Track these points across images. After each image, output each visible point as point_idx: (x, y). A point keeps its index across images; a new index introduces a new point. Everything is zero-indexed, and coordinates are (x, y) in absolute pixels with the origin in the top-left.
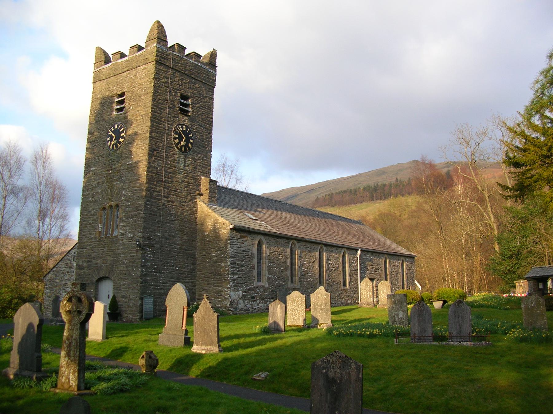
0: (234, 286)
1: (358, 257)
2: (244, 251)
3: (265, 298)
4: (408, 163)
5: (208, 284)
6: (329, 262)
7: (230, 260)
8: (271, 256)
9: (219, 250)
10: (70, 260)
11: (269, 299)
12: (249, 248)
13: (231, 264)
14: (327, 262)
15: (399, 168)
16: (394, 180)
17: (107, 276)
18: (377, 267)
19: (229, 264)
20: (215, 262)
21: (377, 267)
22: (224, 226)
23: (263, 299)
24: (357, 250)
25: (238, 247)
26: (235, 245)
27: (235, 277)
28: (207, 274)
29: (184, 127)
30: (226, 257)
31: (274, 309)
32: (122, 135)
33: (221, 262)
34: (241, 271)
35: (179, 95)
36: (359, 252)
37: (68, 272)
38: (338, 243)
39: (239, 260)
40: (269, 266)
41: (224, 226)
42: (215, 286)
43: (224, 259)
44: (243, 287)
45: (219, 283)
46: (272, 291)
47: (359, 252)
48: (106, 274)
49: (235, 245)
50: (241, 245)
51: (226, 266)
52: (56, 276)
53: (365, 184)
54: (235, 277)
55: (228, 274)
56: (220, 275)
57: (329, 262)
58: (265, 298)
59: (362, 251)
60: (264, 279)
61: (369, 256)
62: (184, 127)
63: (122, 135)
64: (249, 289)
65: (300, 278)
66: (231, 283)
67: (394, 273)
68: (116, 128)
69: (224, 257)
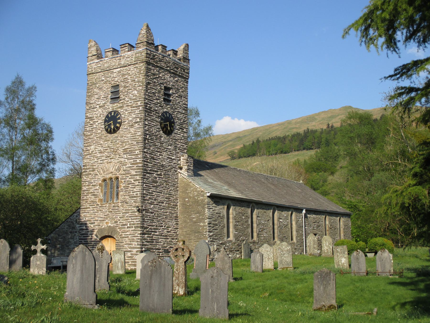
0: (211, 241)
1: (303, 215)
2: (217, 213)
3: (233, 251)
4: (340, 110)
5: (189, 240)
6: (280, 220)
7: (207, 221)
8: (237, 216)
9: (198, 213)
10: (72, 222)
11: (236, 251)
12: (221, 210)
13: (209, 224)
14: (278, 221)
15: (333, 114)
16: (325, 127)
17: (110, 234)
18: (318, 224)
19: (206, 224)
20: (195, 222)
21: (318, 224)
22: (202, 194)
23: (231, 251)
24: (302, 210)
25: (213, 210)
26: (211, 208)
27: (211, 234)
28: (188, 232)
29: (168, 114)
30: (204, 218)
31: (254, 256)
32: (118, 121)
33: (200, 222)
34: (215, 230)
35: (163, 88)
36: (304, 211)
37: (71, 232)
38: (287, 204)
39: (214, 221)
40: (235, 225)
41: (202, 194)
42: (195, 241)
43: (203, 220)
44: (217, 242)
45: (199, 239)
46: (238, 245)
47: (304, 211)
48: (109, 233)
49: (211, 208)
50: (215, 208)
51: (204, 226)
52: (59, 235)
53: (295, 131)
54: (211, 234)
55: (206, 232)
56: (199, 232)
57: (280, 220)
58: (233, 251)
59: (306, 211)
60: (231, 235)
61: (311, 216)
62: (168, 114)
63: (118, 121)
64: (221, 244)
65: (258, 234)
66: (209, 239)
67: (333, 229)
68: (113, 114)
69: (202, 219)
